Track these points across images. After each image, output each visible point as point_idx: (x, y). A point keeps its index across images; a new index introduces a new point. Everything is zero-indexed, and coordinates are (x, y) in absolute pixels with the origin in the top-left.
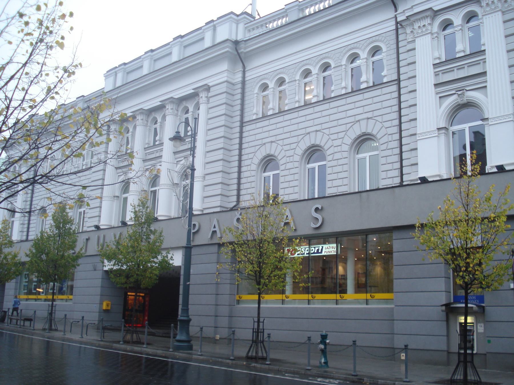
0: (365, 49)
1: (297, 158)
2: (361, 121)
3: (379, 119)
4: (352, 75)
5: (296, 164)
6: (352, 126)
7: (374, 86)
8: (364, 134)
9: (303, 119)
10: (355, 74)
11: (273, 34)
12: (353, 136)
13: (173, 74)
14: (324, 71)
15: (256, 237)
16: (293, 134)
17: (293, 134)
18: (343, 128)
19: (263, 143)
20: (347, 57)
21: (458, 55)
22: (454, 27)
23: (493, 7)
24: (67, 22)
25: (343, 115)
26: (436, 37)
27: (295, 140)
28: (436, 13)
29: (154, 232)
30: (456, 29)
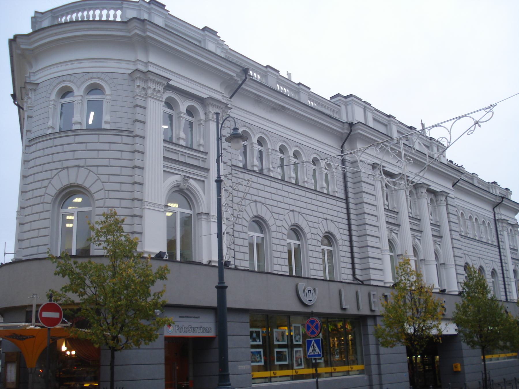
0: (81, 85)
1: (48, 199)
2: (69, 169)
3: (94, 169)
4: (61, 113)
5: (48, 207)
6: (57, 173)
7: (60, 132)
8: (72, 186)
9: (59, 149)
10: (66, 112)
11: (219, 61)
12: (59, 186)
13: (162, 43)
14: (63, 97)
15: (359, 146)
16: (46, 167)
17: (46, 167)
18: (48, 175)
19: (64, 166)
20: (58, 89)
21: (75, 127)
22: (73, 96)
23: (159, 96)
24: (423, 125)
25: (49, 159)
26: (81, 100)
27: (48, 175)
28: (169, 87)
29: (55, 262)
30: (76, 98)
